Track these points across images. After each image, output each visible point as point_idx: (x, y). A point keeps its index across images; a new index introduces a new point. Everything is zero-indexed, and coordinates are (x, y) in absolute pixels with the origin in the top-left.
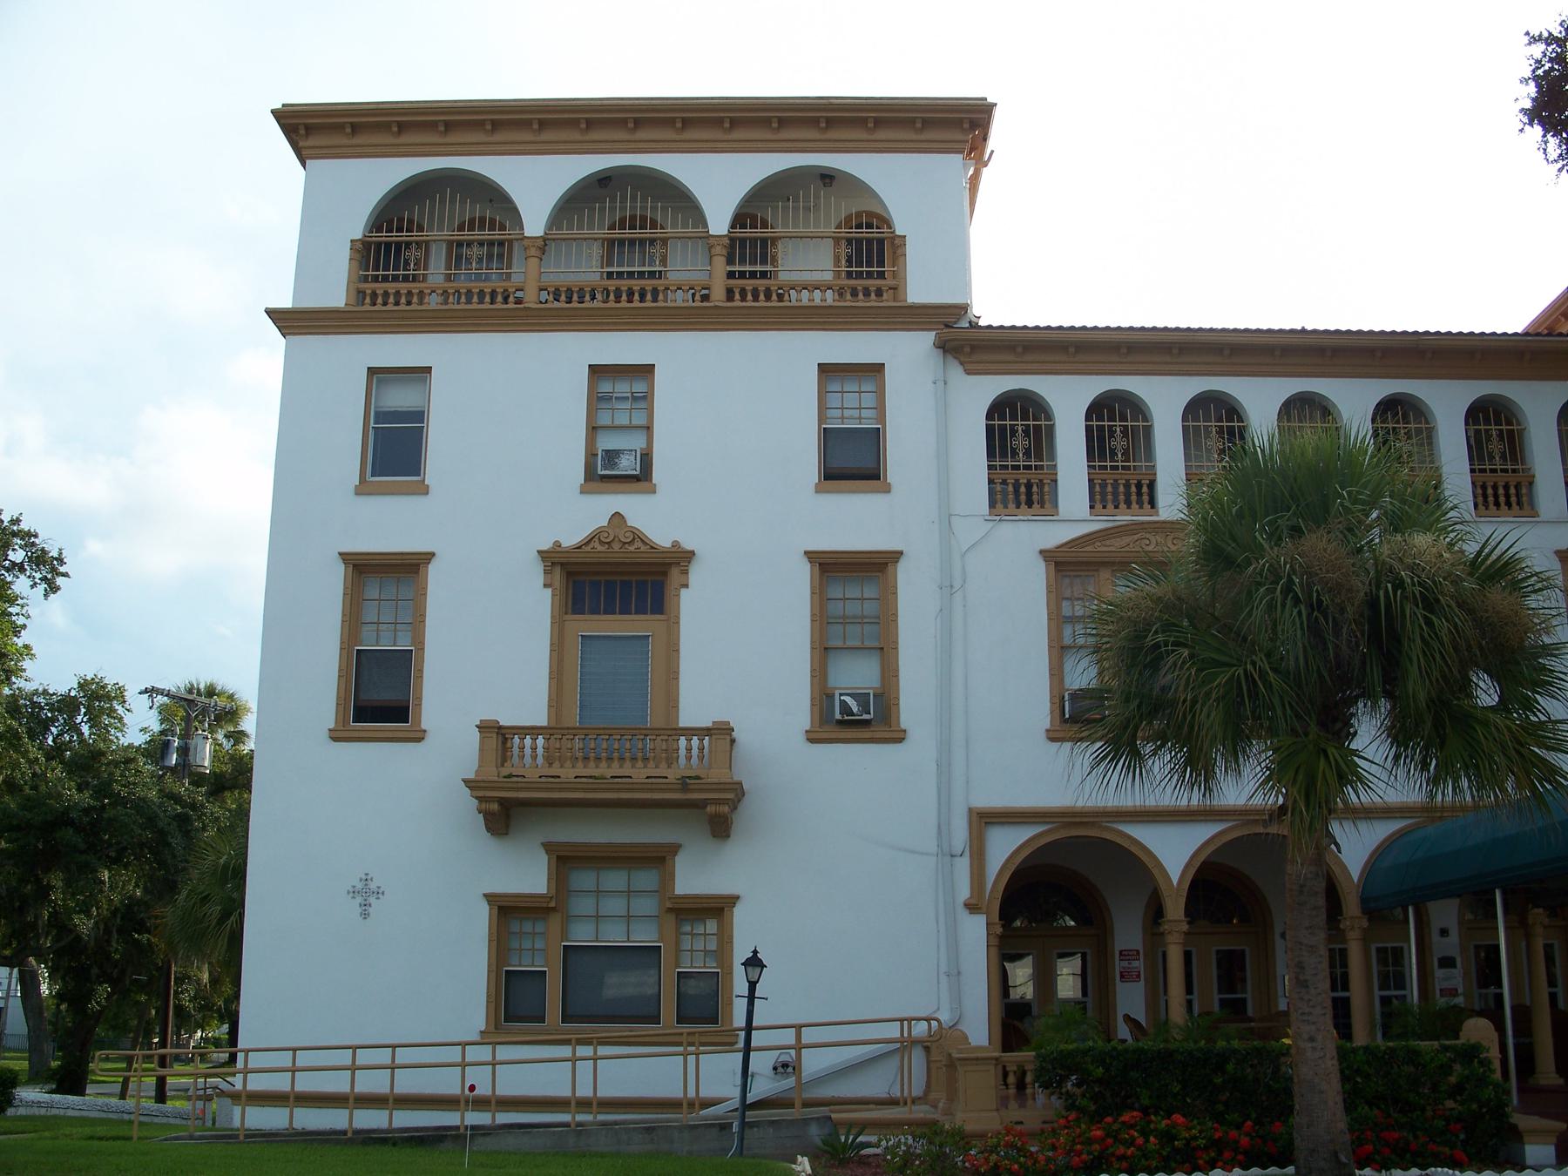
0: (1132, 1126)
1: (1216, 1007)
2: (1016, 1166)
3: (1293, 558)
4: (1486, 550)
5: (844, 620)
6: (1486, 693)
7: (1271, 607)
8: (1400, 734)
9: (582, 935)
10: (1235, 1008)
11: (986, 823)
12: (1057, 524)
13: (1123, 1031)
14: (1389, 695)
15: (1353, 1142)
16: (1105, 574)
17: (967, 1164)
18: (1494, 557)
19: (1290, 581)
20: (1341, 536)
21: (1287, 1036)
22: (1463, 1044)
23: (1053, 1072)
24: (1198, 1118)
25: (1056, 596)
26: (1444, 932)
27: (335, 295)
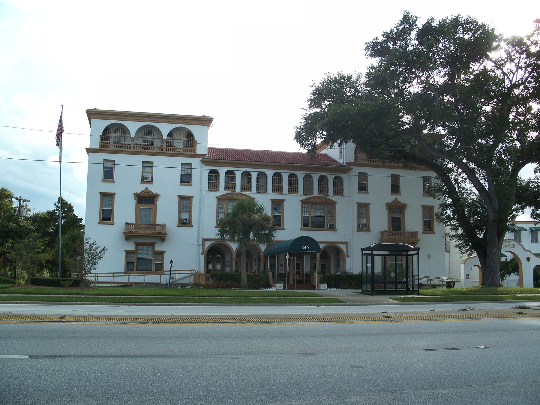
5: (184, 207)
9: (140, 257)
25: (218, 204)
26: (281, 260)
27: (97, 146)
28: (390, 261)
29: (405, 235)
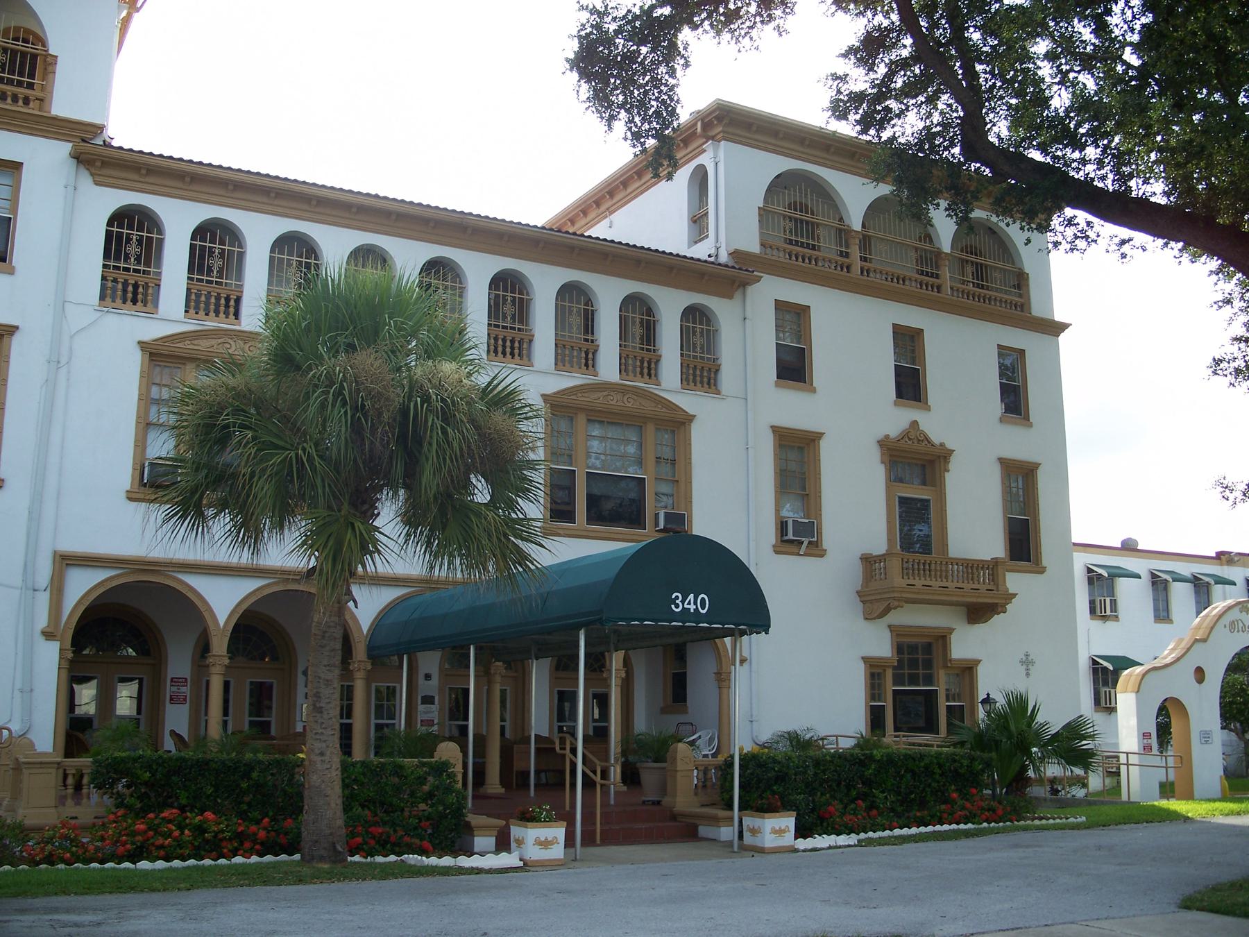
0: (170, 821)
1: (246, 727)
2: (68, 855)
3: (345, 369)
4: (495, 382)
6: (481, 493)
7: (323, 406)
8: (411, 519)
10: (263, 728)
11: (67, 564)
12: (155, 321)
13: (169, 744)
14: (407, 487)
15: (347, 836)
16: (190, 367)
17: (24, 854)
18: (500, 388)
19: (342, 386)
20: (385, 355)
21: (302, 752)
22: (436, 762)
23: (106, 776)
24: (226, 815)
25: (147, 380)
28: (894, 684)
29: (947, 571)
